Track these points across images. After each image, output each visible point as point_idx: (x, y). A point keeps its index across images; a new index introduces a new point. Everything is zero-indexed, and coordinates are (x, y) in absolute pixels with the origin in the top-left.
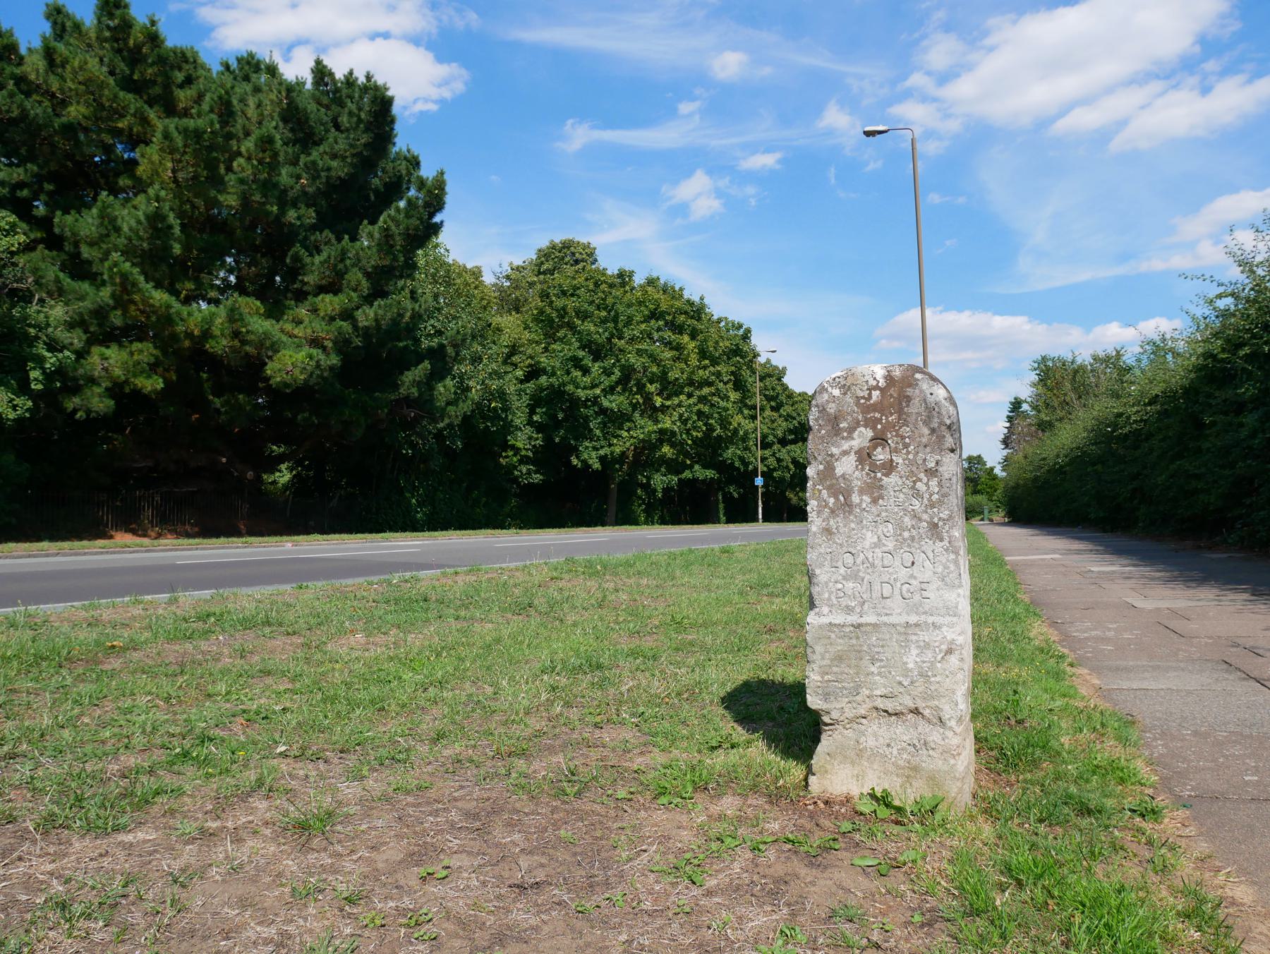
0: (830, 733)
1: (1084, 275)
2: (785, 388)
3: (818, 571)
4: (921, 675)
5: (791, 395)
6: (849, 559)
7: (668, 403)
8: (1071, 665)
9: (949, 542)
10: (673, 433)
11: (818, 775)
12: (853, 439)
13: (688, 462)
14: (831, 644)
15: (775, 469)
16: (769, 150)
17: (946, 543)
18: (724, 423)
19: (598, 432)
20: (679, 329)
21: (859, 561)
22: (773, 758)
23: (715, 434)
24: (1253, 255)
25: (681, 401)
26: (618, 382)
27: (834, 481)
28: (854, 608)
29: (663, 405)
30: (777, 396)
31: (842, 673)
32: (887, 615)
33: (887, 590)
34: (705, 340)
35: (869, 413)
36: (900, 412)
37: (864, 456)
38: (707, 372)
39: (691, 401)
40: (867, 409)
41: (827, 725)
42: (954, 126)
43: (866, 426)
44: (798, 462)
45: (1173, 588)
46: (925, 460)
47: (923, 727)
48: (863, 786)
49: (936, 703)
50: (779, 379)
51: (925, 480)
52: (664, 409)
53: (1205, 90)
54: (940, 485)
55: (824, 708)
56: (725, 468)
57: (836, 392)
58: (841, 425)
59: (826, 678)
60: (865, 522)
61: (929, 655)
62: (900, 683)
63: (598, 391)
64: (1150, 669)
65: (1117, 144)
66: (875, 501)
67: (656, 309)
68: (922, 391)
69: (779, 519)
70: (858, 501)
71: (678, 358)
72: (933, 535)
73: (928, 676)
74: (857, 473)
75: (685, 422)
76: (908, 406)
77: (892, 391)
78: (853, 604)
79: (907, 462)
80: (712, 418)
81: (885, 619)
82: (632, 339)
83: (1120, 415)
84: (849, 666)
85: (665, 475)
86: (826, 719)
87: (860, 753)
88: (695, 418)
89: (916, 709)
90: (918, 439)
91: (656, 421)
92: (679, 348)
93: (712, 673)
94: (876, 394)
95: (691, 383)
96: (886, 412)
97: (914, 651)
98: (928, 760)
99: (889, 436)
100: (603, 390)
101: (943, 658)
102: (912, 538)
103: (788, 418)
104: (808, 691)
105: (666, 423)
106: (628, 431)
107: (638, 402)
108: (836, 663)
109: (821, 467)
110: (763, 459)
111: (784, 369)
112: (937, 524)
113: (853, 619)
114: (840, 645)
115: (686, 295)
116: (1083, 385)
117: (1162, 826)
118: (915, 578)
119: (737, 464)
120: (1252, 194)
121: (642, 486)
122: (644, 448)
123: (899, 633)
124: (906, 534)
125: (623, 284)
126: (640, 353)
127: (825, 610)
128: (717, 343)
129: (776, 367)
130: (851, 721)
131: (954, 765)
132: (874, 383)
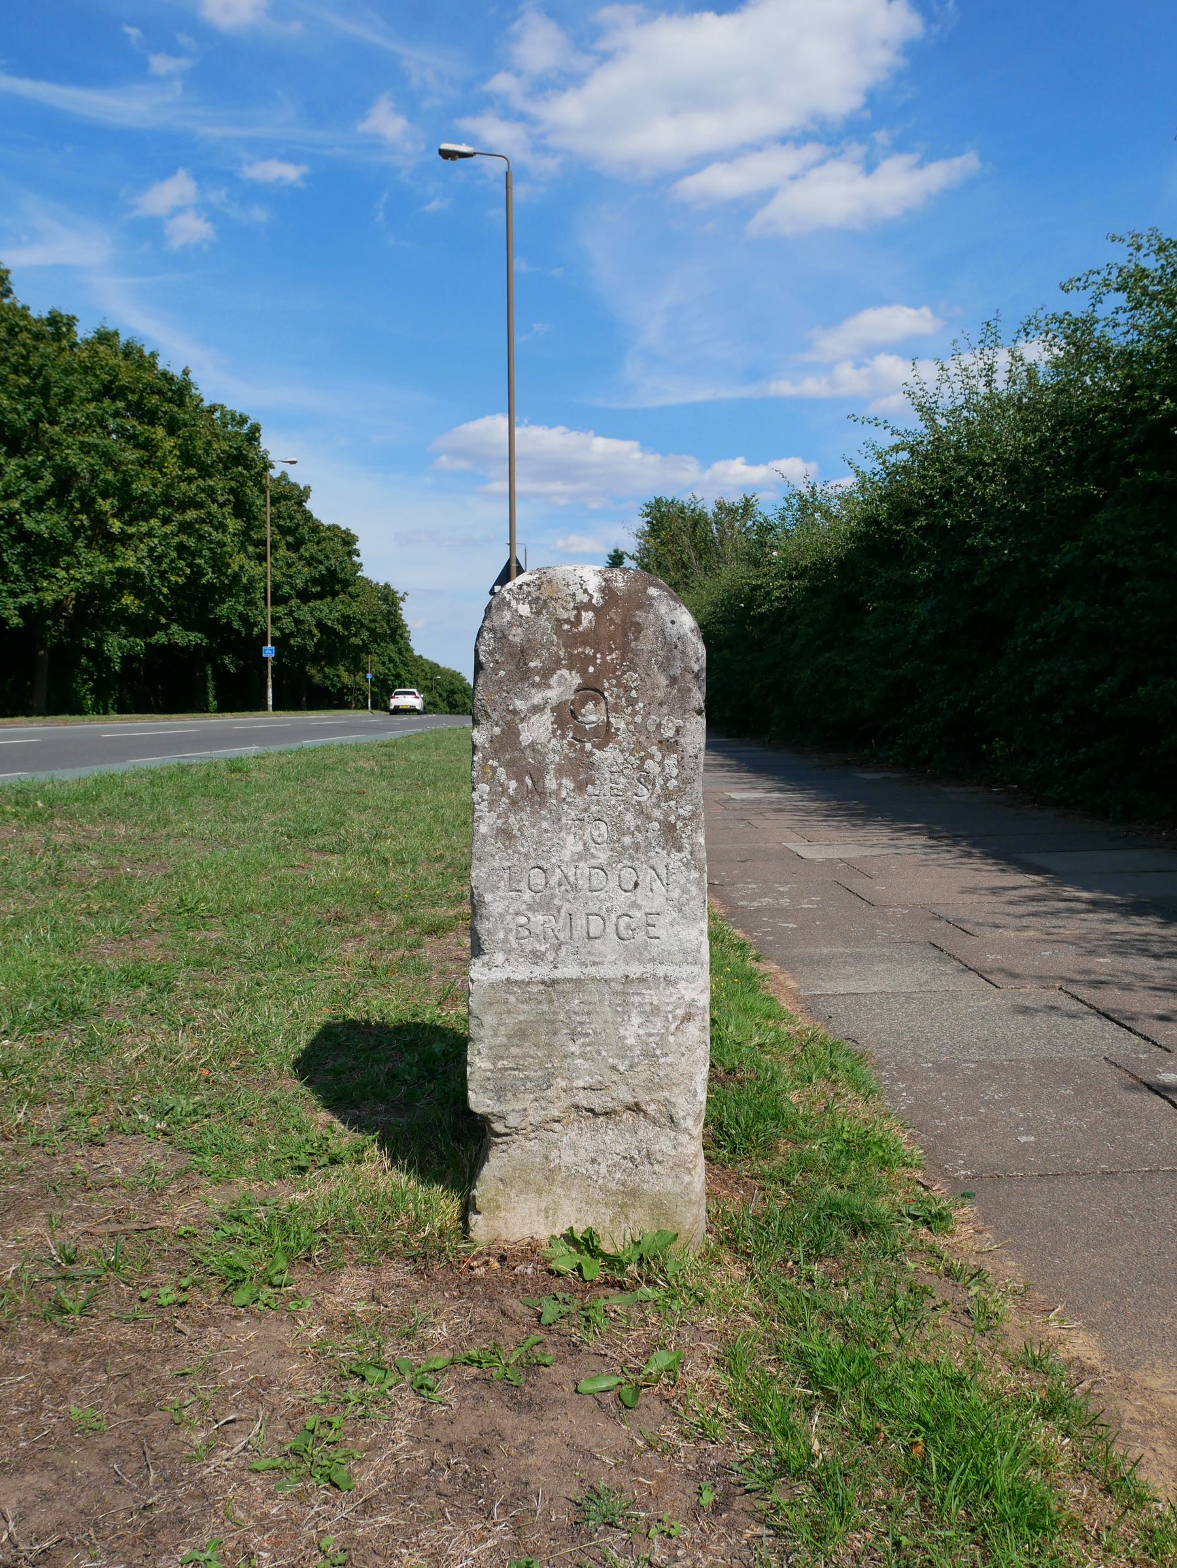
0: (504, 1147)
1: (703, 394)
2: (308, 517)
3: (488, 897)
4: (645, 1054)
5: (316, 528)
6: (538, 878)
7: (131, 530)
8: (757, 959)
9: (692, 853)
10: (139, 576)
11: (485, 1213)
12: (549, 687)
13: (163, 621)
14: (509, 1012)
15: (292, 635)
16: (290, 157)
17: (686, 854)
18: (219, 564)
19: (16, 568)
20: (149, 417)
21: (553, 881)
22: (403, 1180)
23: (204, 581)
24: (935, 398)
25: (152, 529)
26: (49, 493)
27: (517, 754)
28: (544, 954)
29: (123, 532)
30: (296, 529)
31: (525, 1056)
32: (594, 963)
33: (596, 926)
34: (191, 438)
35: (577, 648)
36: (625, 648)
37: (567, 716)
38: (193, 487)
39: (168, 529)
40: (573, 640)
41: (499, 1135)
42: (550, 165)
43: (570, 668)
44: (326, 625)
45: (837, 827)
46: (659, 725)
47: (646, 1131)
48: (554, 1225)
49: (666, 1094)
50: (300, 504)
51: (658, 756)
52: (124, 539)
53: (870, 167)
54: (681, 765)
55: (495, 1110)
56: (213, 628)
57: (524, 610)
58: (532, 665)
59: (500, 1064)
60: (564, 821)
61: (658, 1024)
62: (614, 1068)
63: (16, 504)
64: (850, 959)
65: (755, 226)
66: (580, 787)
67: (112, 382)
68: (658, 617)
69: (296, 706)
70: (554, 787)
71: (148, 462)
72: (667, 841)
73: (655, 1056)
74: (554, 741)
75: (158, 560)
76: (636, 639)
77: (612, 613)
78: (543, 949)
80: (200, 556)
81: (592, 971)
82: (73, 426)
83: (757, 588)
84: (537, 1046)
85: (125, 638)
86: (498, 1127)
87: (550, 1176)
88: (174, 554)
89: (636, 1104)
90: (650, 692)
91: (112, 557)
92: (148, 445)
93: (271, 1015)
94: (587, 617)
95: (167, 501)
96: (603, 647)
97: (636, 1020)
98: (653, 1180)
99: (606, 685)
100: (24, 503)
101: (677, 1028)
102: (636, 847)
103: (312, 561)
104: (470, 1085)
105: (129, 560)
106: (67, 569)
107: (82, 525)
108: (516, 1041)
109: (497, 730)
110: (275, 620)
111: (307, 490)
112: (674, 826)
113: (542, 971)
114: (524, 1013)
115: (161, 364)
116: (704, 540)
117: (956, 1240)
118: (639, 907)
119: (236, 625)
120: (907, 310)
121: (88, 652)
122: (92, 597)
123: (615, 993)
124: (627, 840)
125: (58, 337)
126: (86, 448)
127: (500, 957)
128: (209, 443)
129: (296, 486)
130: (537, 1127)
131: (690, 1184)
132: (585, 599)
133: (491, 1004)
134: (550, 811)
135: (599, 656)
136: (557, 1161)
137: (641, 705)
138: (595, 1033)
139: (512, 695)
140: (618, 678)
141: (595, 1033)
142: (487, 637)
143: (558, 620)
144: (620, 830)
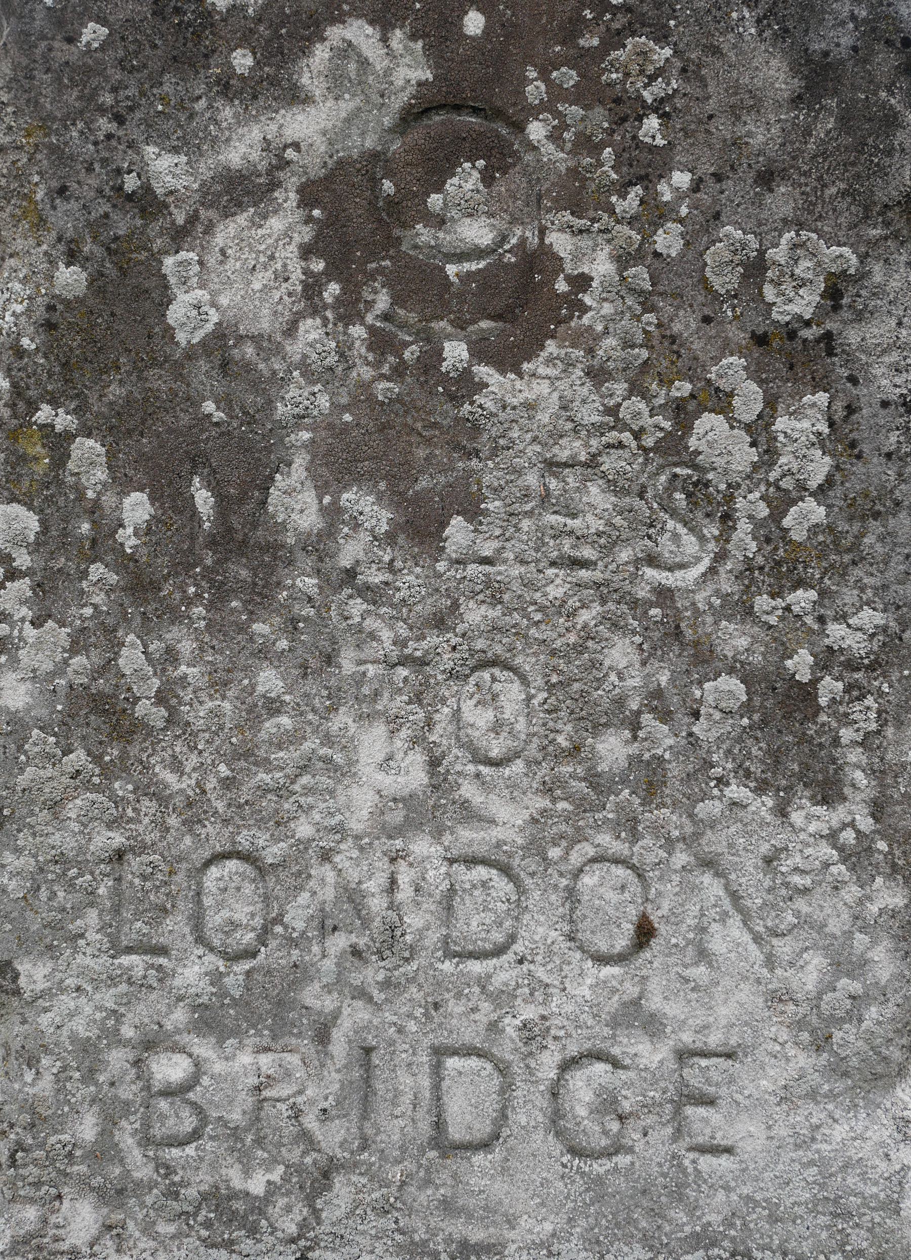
9: (877, 809)
60: (347, 663)
72: (776, 757)
78: (257, 1185)
79: (640, 275)
90: (722, 128)
99: (536, 90)
112: (808, 692)
134: (292, 625)
137: (682, 179)
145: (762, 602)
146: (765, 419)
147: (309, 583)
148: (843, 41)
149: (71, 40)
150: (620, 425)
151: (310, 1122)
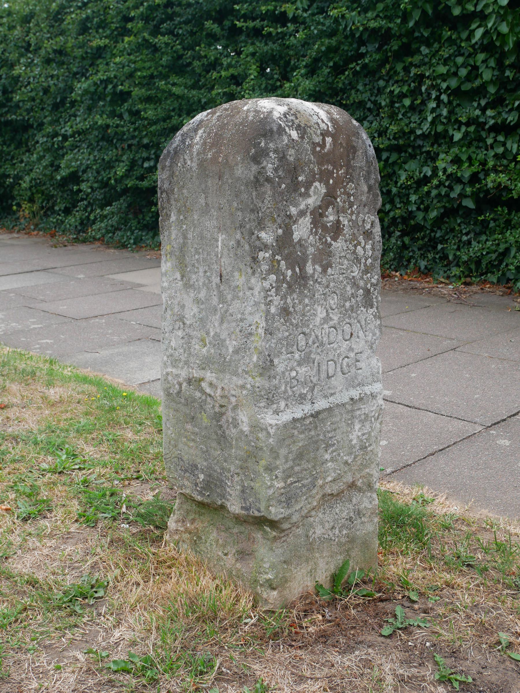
12: (309, 196)
27: (291, 249)
35: (324, 165)
57: (294, 134)
59: (289, 482)
78: (305, 392)
97: (357, 426)
112: (369, 290)
113: (308, 408)
114: (301, 440)
124: (348, 304)
133: (284, 440)
134: (309, 291)
135: (335, 171)
136: (313, 536)
137: (355, 207)
138: (338, 442)
139: (289, 204)
140: (345, 187)
141: (338, 442)
142: (273, 157)
143: (313, 143)
144: (345, 298)
145: (365, 277)
146: (365, 246)
147: (311, 283)
148: (53, 392)
149: (280, 187)
150: (349, 249)
151: (312, 378)
